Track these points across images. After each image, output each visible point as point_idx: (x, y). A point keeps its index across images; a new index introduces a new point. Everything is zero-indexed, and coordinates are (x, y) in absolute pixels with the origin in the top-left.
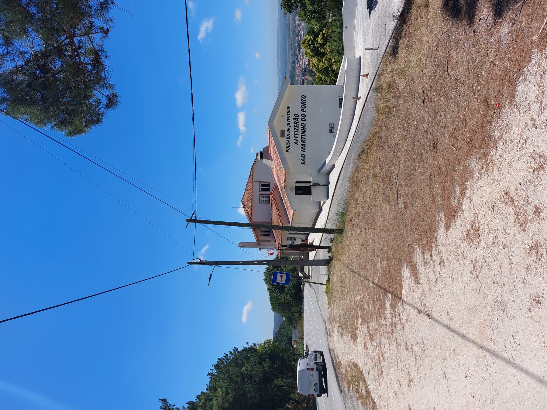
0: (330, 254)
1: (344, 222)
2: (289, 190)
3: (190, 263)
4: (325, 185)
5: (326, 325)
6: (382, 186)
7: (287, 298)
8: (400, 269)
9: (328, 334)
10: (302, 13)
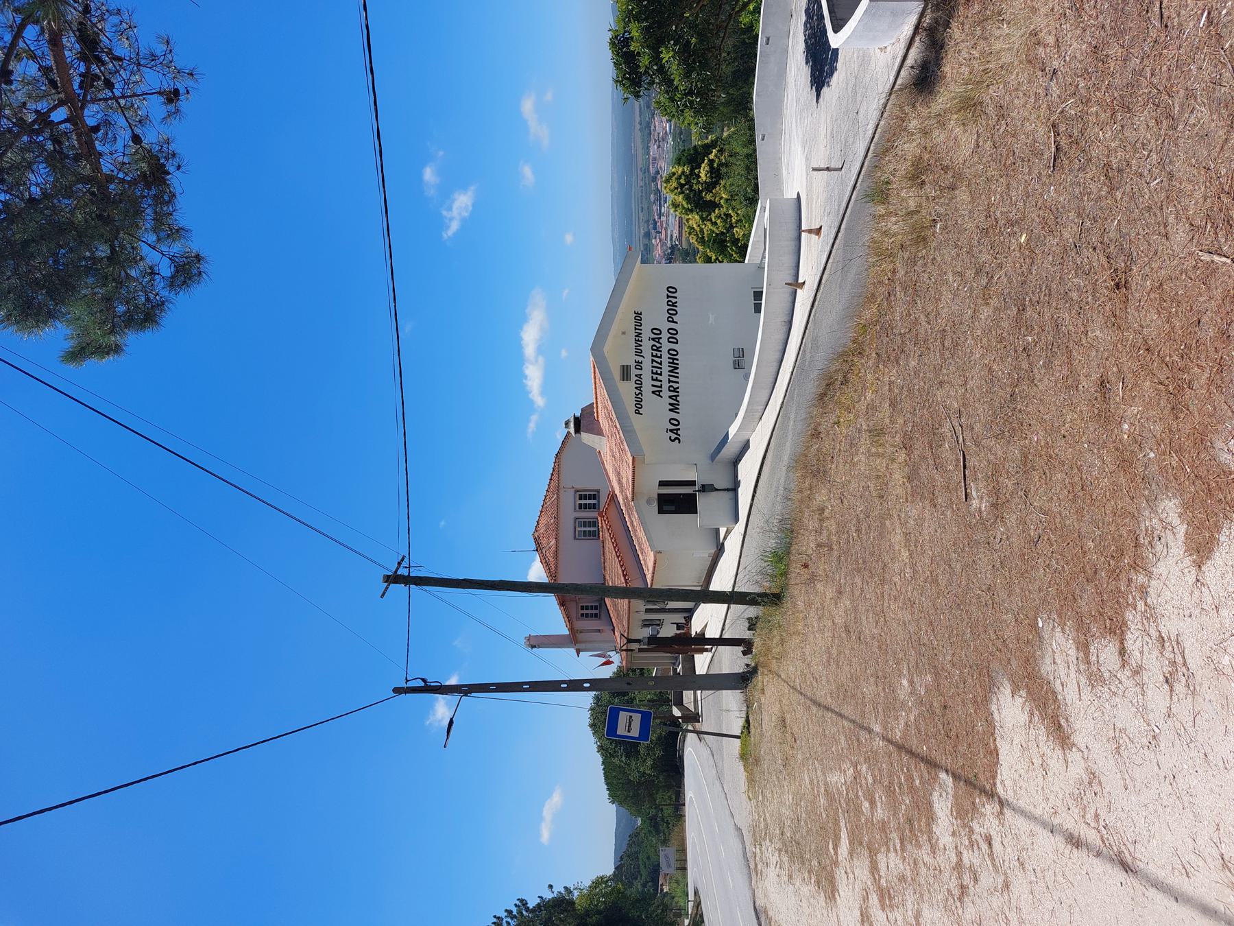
0: (747, 659)
1: (785, 574)
2: (643, 502)
3: (398, 691)
4: (728, 490)
5: (743, 843)
6: (902, 456)
7: (646, 774)
8: (986, 700)
9: (752, 870)
10: (663, 99)
